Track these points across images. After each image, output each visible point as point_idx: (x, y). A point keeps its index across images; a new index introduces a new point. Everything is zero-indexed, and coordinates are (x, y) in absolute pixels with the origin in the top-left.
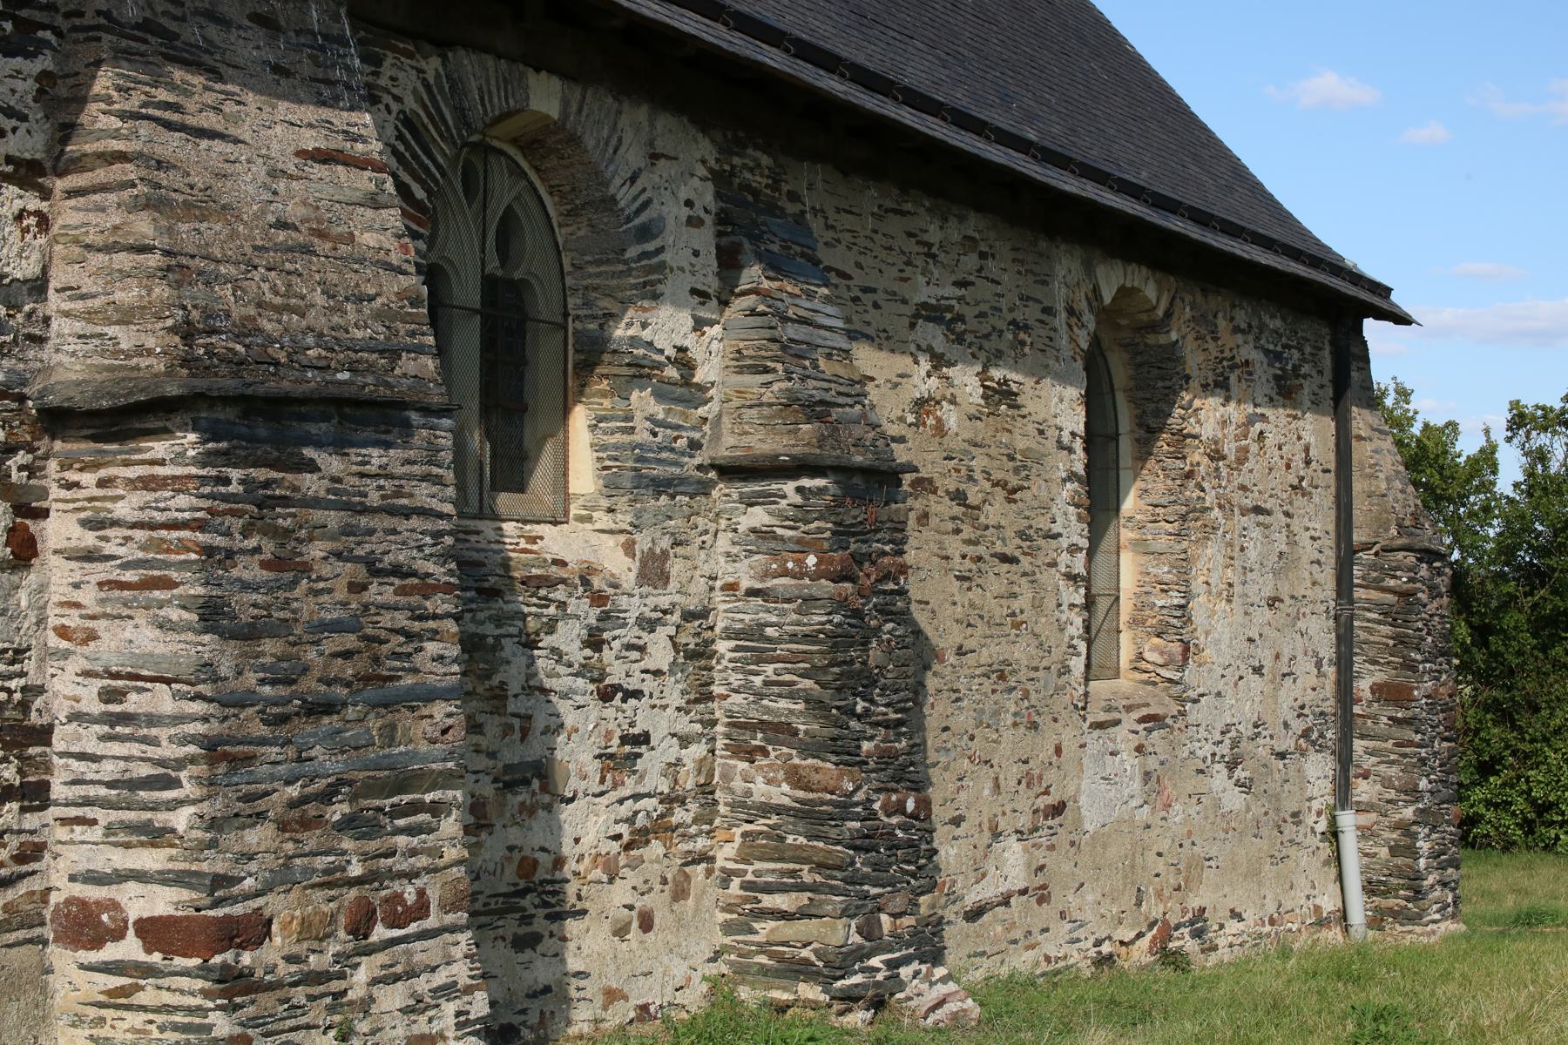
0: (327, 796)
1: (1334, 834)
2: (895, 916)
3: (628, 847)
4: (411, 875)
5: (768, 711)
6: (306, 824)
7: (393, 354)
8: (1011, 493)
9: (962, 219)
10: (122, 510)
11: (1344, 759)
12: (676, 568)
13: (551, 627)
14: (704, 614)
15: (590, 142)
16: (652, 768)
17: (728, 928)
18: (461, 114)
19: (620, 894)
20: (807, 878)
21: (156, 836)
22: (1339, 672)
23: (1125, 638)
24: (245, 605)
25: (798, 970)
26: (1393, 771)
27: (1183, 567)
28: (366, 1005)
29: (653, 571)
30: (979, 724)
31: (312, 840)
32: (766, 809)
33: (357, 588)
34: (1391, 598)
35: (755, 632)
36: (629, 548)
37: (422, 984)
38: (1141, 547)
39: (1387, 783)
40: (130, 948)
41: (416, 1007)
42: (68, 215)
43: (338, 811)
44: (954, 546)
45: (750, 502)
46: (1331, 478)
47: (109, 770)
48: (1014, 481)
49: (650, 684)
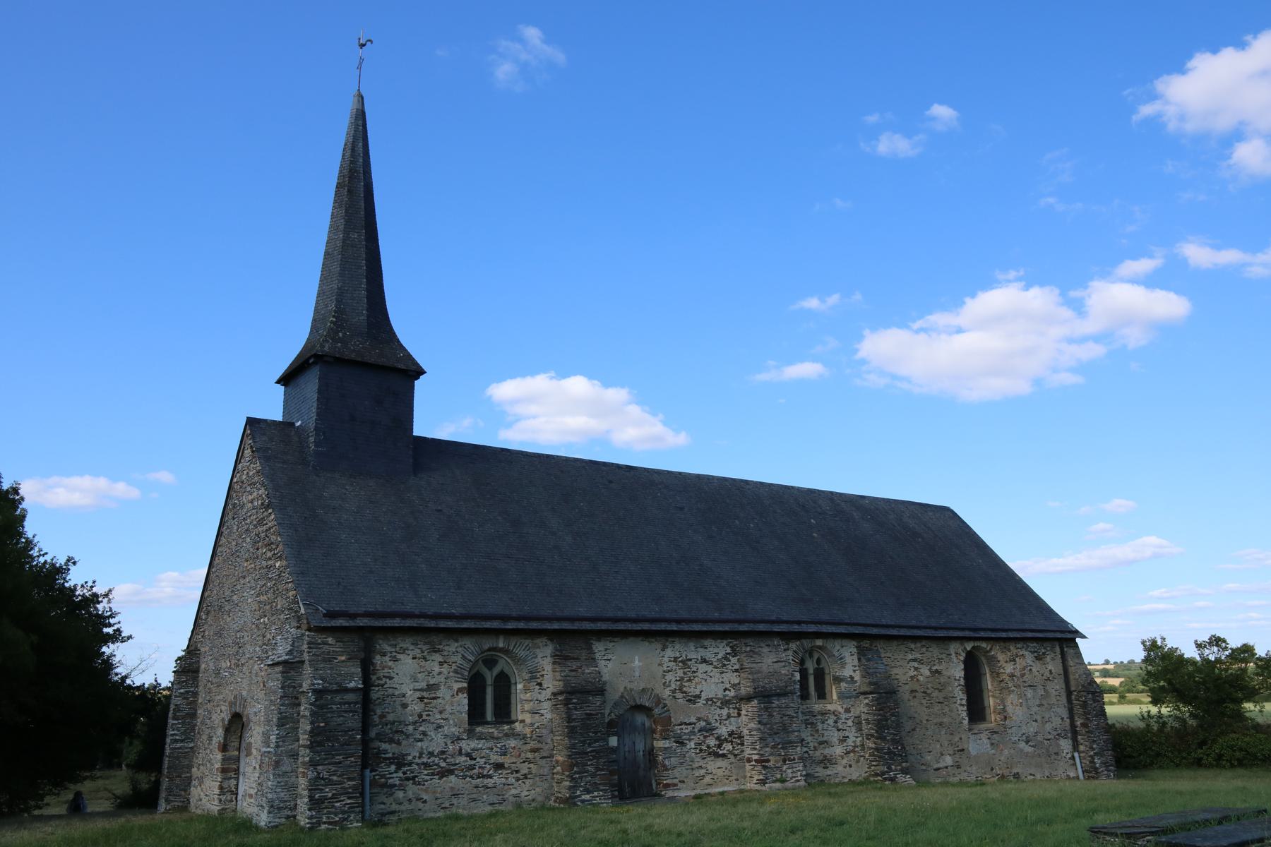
0: (778, 744)
1: (1073, 758)
2: (896, 766)
3: (845, 754)
4: (792, 755)
5: (594, 747)
6: (775, 748)
7: (787, 687)
8: (940, 691)
9: (920, 642)
10: (750, 710)
11: (1075, 740)
12: (852, 710)
13: (827, 720)
14: (859, 717)
15: (828, 647)
16: (850, 742)
17: (868, 768)
18: (804, 649)
19: (845, 761)
20: (878, 759)
21: (755, 749)
22: (1070, 721)
23: (992, 715)
24: (764, 721)
25: (877, 775)
26: (1087, 743)
27: (1003, 700)
28: (785, 772)
29: (847, 710)
30: (934, 734)
31: (776, 750)
32: (872, 748)
33: (782, 718)
34: (1081, 703)
35: (867, 719)
36: (842, 708)
37: (794, 769)
38: (993, 696)
39: (1086, 746)
40: (753, 763)
41: (794, 772)
42: (742, 675)
43: (780, 746)
44: (924, 701)
45: (865, 698)
46: (1062, 676)
47: (750, 741)
48: (941, 688)
49: (848, 728)
